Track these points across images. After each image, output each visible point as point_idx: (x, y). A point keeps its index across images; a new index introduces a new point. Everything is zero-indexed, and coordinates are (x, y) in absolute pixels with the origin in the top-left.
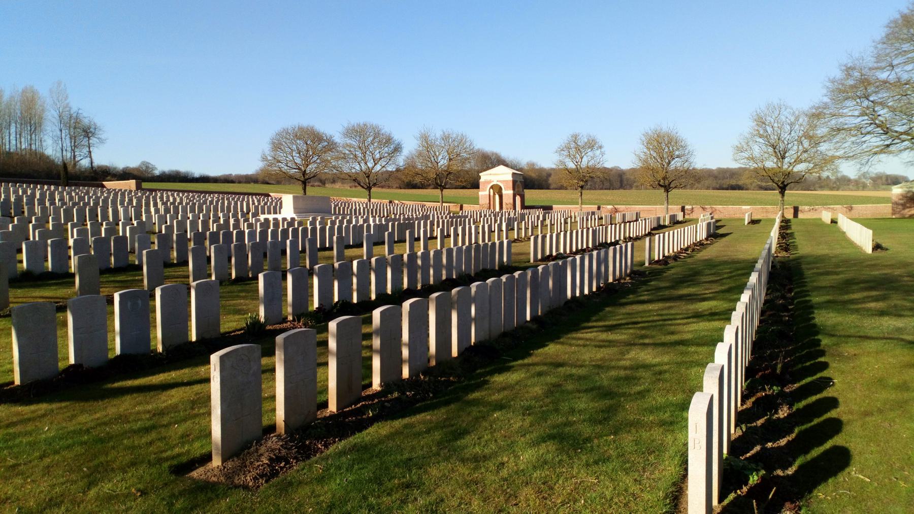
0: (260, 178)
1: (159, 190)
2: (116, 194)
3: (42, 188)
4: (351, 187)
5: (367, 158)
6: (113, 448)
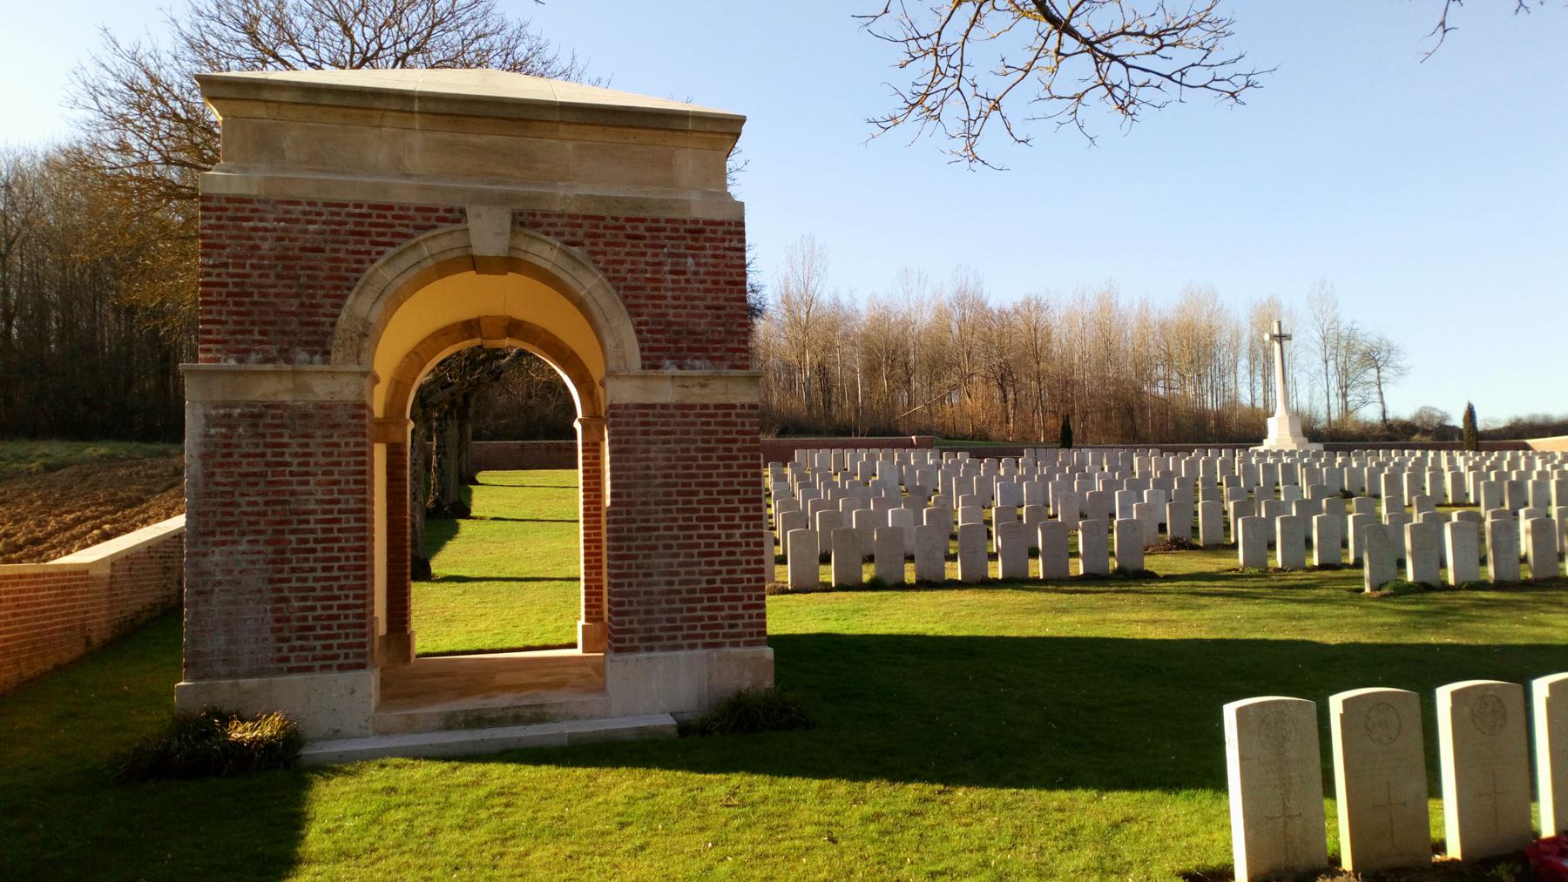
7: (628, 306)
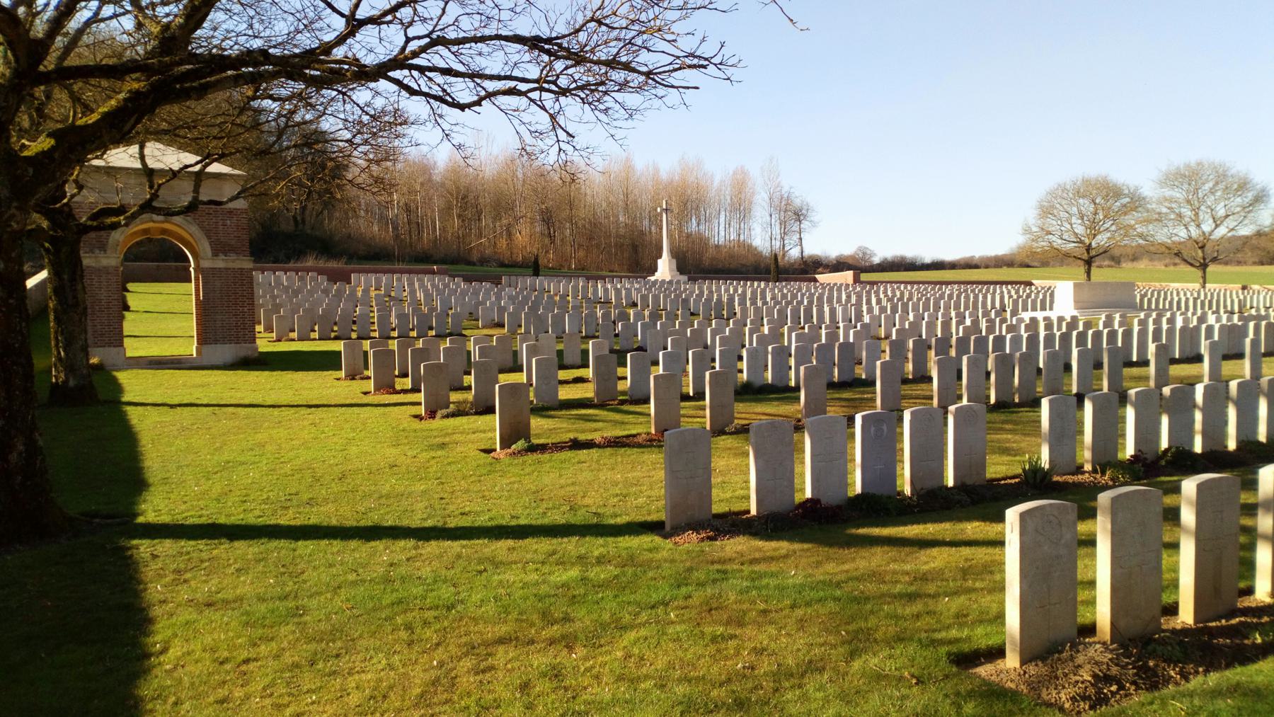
0: (1018, 259)
1: (882, 282)
2: (831, 290)
3: (752, 286)
4: (1166, 266)
5: (1201, 218)
6: (872, 612)
7: (207, 236)
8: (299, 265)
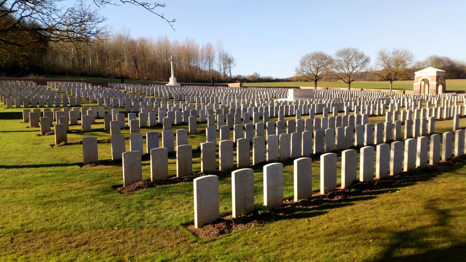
8: (27, 78)
